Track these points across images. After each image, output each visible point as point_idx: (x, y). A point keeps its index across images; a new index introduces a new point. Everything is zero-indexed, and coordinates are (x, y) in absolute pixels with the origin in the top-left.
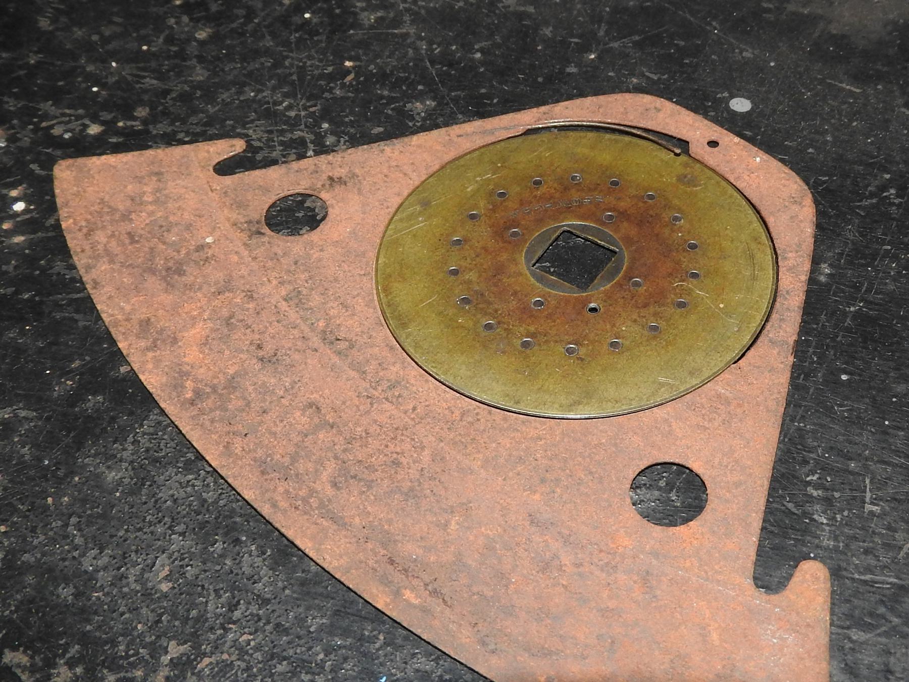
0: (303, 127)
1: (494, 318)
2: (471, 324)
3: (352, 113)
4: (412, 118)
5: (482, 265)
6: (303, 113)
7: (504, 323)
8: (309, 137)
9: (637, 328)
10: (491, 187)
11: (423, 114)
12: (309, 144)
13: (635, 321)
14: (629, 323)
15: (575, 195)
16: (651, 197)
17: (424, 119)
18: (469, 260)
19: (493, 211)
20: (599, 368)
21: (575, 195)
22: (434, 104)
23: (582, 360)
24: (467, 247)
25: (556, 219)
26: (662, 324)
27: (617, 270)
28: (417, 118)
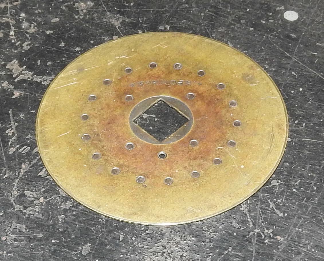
0: (8, 15)
1: (101, 151)
2: (85, 153)
3: (40, 7)
4: (78, 13)
5: (103, 115)
6: (9, 6)
7: (106, 155)
8: (12, 22)
9: (185, 172)
10: (123, 64)
11: (85, 11)
12: (12, 27)
13: (185, 167)
14: (181, 168)
15: (174, 78)
16: (222, 87)
17: (85, 15)
18: (96, 112)
19: (120, 80)
20: (154, 194)
21: (174, 78)
22: (92, 4)
23: (146, 187)
24: (97, 102)
25: (157, 92)
26: (202, 172)
27: (185, 132)
28: (81, 13)
